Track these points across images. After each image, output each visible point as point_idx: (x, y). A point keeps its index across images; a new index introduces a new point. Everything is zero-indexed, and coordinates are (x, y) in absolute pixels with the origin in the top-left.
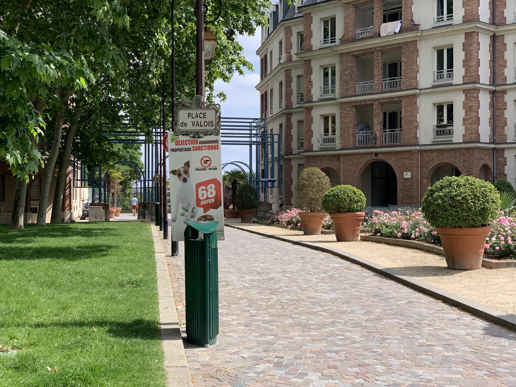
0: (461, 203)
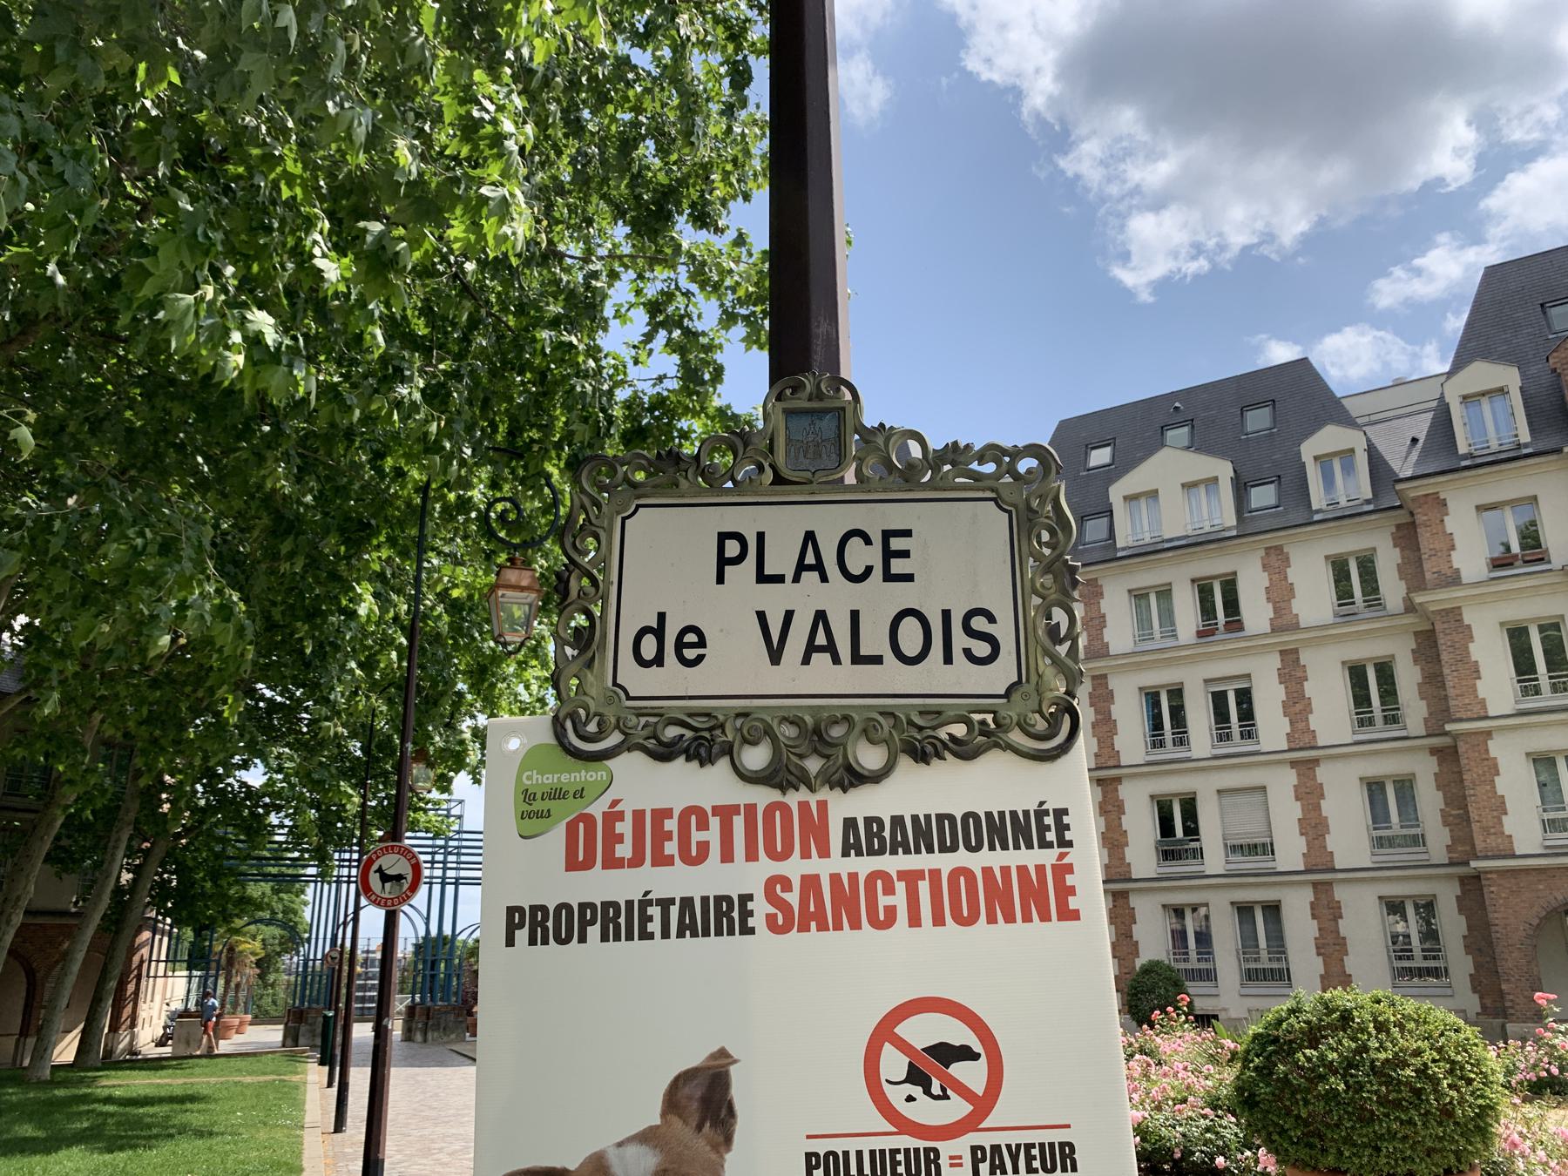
0: (1418, 1093)
